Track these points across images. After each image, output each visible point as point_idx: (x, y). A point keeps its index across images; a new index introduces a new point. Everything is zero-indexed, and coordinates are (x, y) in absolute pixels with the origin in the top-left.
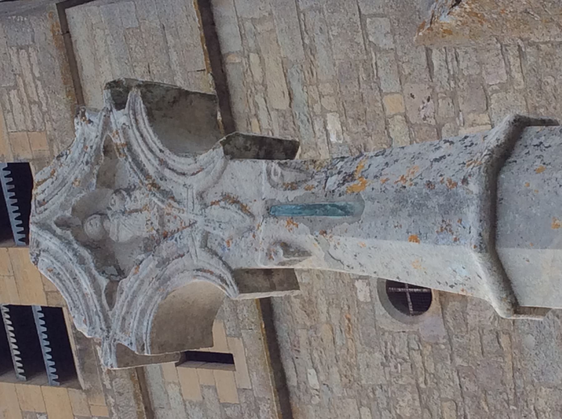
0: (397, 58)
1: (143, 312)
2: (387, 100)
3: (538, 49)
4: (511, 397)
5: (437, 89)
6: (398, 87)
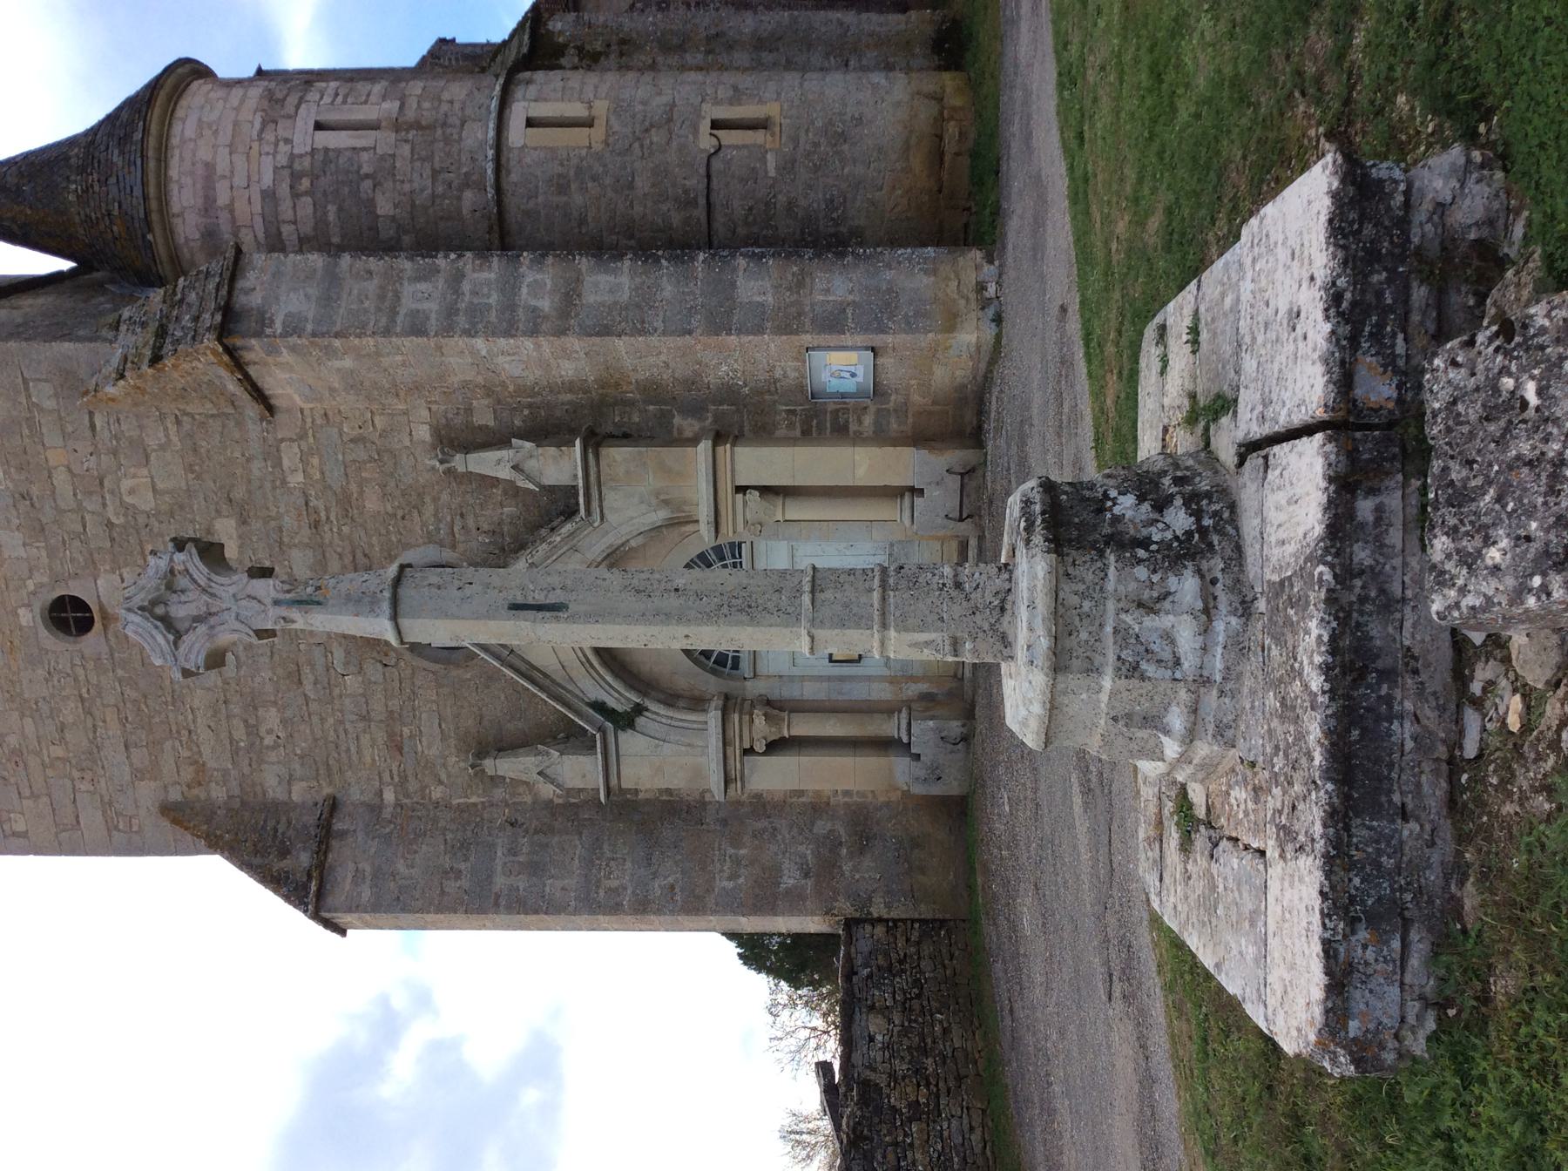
0: (61, 418)
1: (198, 652)
2: (49, 454)
3: (193, 417)
4: (169, 699)
5: (100, 446)
6: (61, 443)
